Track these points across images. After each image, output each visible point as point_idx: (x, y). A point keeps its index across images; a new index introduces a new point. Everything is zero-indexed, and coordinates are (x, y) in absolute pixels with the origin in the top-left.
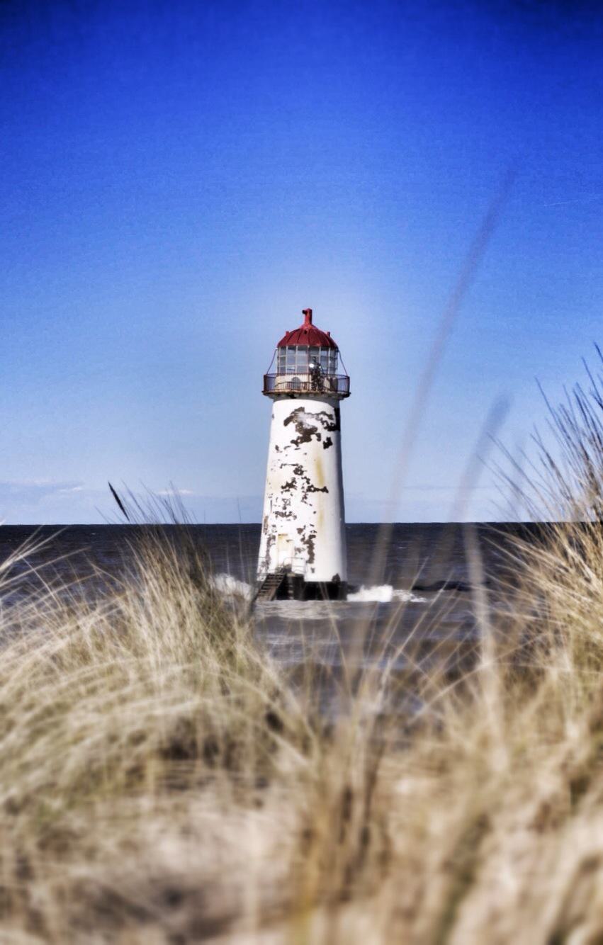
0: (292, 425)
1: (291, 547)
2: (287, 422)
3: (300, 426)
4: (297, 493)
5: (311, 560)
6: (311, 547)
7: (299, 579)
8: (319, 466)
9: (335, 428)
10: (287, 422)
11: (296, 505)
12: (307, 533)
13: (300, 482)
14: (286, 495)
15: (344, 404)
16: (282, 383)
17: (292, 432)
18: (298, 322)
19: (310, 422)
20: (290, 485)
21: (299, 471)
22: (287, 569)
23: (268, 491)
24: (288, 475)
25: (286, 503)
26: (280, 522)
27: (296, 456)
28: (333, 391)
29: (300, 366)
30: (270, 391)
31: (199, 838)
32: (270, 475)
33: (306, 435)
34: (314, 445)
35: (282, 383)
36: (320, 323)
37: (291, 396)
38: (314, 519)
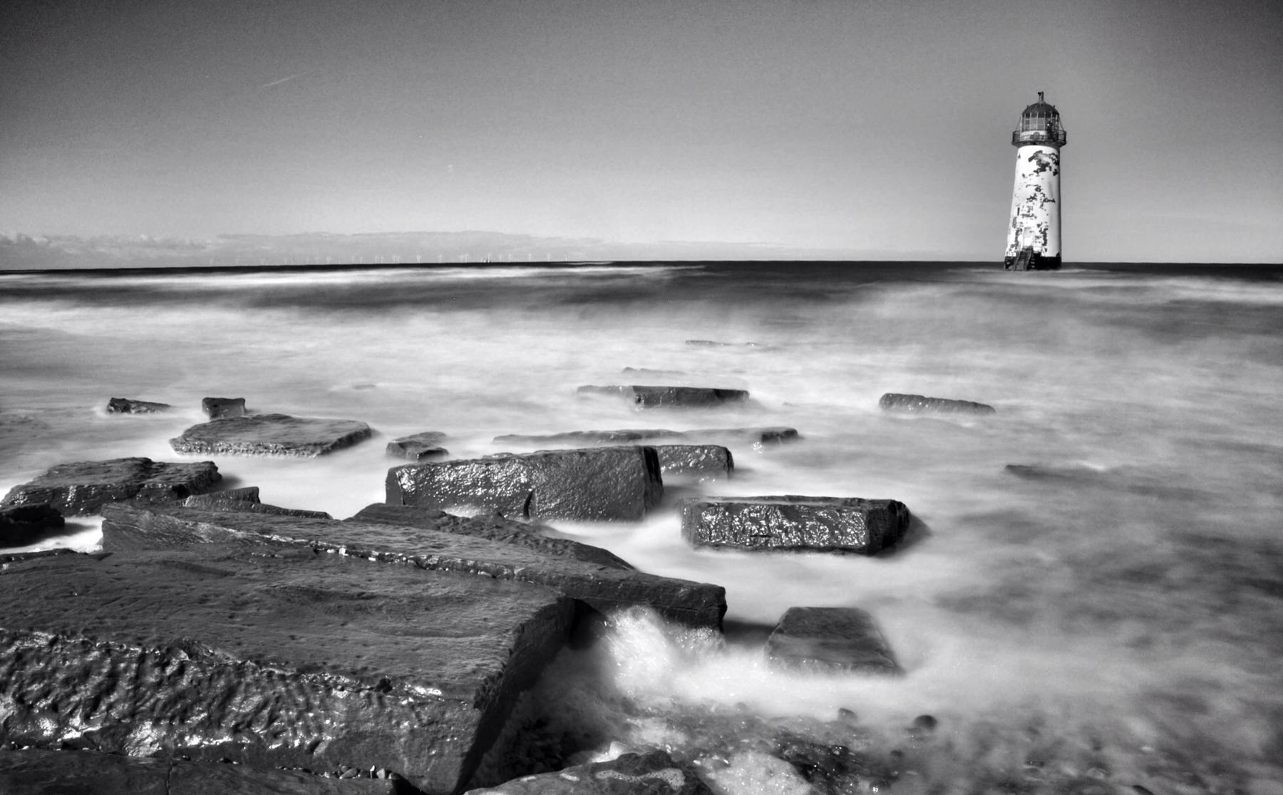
0: (1034, 162)
1: (1032, 236)
2: (1030, 160)
3: (1039, 162)
4: (1038, 203)
5: (1045, 244)
6: (1045, 236)
8: (1050, 186)
9: (1057, 163)
10: (1030, 160)
11: (1036, 209)
12: (1043, 227)
13: (1039, 196)
14: (1030, 204)
15: (1062, 149)
17: (1034, 165)
18: (1035, 100)
19: (1046, 160)
20: (1033, 198)
21: (1038, 189)
22: (1030, 248)
24: (1031, 191)
25: (1030, 209)
26: (1025, 220)
27: (1036, 180)
28: (1055, 139)
31: (169, 493)
32: (1016, 191)
33: (1043, 167)
34: (1047, 174)
35: (1026, 135)
36: (1049, 100)
37: (1034, 143)
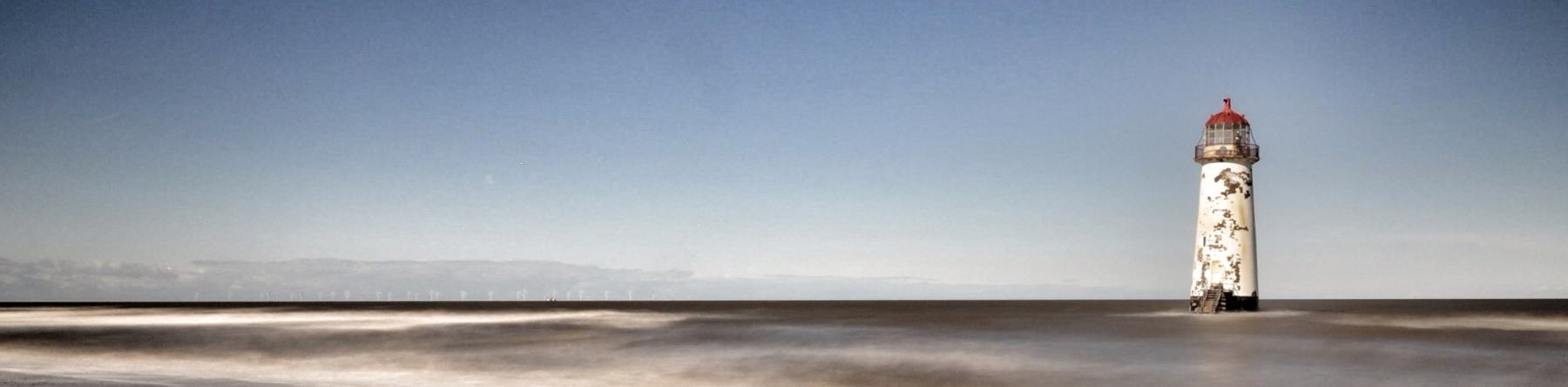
0: (1221, 182)
2: (1217, 179)
4: (1227, 231)
5: (1237, 281)
7: (1229, 295)
8: (1242, 211)
9: (1250, 184)
10: (1217, 179)
12: (1234, 260)
13: (1229, 223)
15: (1254, 166)
16: (1210, 151)
17: (1222, 186)
18: (1221, 108)
19: (1235, 179)
20: (1221, 225)
21: (1227, 214)
22: (1220, 286)
23: (1200, 229)
25: (1218, 239)
28: (1247, 154)
29: (1223, 141)
30: (1201, 159)
32: (1201, 217)
33: (1233, 188)
34: (1237, 197)
35: (1210, 151)
36: (1237, 109)
37: (1221, 160)
38: (1239, 250)
